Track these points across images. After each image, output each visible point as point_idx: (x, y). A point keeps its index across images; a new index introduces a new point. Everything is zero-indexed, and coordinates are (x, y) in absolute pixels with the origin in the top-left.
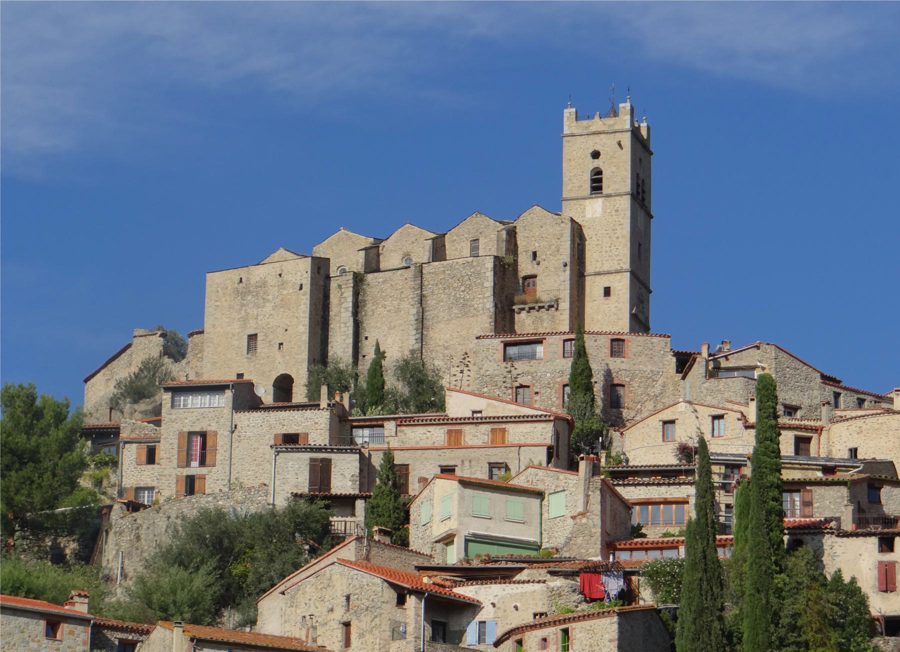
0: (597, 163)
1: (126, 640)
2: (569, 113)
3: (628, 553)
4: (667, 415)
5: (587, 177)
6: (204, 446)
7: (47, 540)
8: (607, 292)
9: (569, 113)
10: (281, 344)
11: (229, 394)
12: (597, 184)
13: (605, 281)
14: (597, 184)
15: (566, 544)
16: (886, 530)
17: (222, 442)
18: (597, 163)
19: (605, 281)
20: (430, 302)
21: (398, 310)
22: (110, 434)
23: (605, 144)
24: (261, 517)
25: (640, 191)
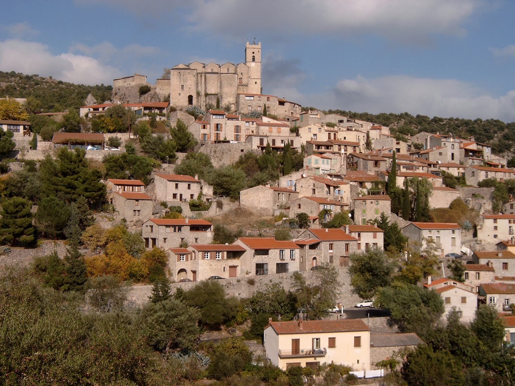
0: (254, 55)
1: (112, 137)
2: (248, 43)
3: (494, 173)
4: (309, 127)
5: (252, 57)
6: (317, 343)
7: (91, 117)
8: (256, 83)
9: (248, 43)
10: (165, 239)
11: (493, 189)
12: (254, 60)
13: (255, 80)
14: (254, 60)
15: (233, 191)
16: (408, 171)
17: (223, 126)
18: (254, 55)
19: (255, 80)
20: (223, 83)
21: (214, 83)
22: (377, 365)
23: (256, 51)
24: (191, 292)
25: (323, 149)
